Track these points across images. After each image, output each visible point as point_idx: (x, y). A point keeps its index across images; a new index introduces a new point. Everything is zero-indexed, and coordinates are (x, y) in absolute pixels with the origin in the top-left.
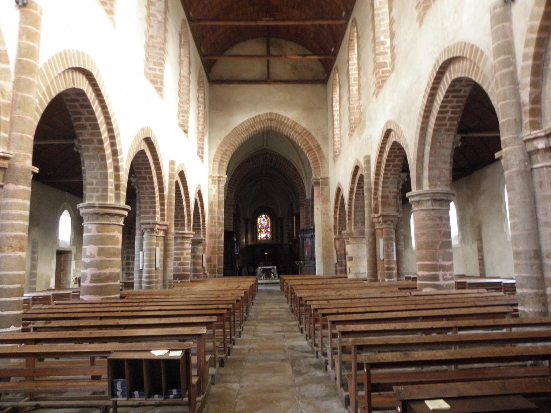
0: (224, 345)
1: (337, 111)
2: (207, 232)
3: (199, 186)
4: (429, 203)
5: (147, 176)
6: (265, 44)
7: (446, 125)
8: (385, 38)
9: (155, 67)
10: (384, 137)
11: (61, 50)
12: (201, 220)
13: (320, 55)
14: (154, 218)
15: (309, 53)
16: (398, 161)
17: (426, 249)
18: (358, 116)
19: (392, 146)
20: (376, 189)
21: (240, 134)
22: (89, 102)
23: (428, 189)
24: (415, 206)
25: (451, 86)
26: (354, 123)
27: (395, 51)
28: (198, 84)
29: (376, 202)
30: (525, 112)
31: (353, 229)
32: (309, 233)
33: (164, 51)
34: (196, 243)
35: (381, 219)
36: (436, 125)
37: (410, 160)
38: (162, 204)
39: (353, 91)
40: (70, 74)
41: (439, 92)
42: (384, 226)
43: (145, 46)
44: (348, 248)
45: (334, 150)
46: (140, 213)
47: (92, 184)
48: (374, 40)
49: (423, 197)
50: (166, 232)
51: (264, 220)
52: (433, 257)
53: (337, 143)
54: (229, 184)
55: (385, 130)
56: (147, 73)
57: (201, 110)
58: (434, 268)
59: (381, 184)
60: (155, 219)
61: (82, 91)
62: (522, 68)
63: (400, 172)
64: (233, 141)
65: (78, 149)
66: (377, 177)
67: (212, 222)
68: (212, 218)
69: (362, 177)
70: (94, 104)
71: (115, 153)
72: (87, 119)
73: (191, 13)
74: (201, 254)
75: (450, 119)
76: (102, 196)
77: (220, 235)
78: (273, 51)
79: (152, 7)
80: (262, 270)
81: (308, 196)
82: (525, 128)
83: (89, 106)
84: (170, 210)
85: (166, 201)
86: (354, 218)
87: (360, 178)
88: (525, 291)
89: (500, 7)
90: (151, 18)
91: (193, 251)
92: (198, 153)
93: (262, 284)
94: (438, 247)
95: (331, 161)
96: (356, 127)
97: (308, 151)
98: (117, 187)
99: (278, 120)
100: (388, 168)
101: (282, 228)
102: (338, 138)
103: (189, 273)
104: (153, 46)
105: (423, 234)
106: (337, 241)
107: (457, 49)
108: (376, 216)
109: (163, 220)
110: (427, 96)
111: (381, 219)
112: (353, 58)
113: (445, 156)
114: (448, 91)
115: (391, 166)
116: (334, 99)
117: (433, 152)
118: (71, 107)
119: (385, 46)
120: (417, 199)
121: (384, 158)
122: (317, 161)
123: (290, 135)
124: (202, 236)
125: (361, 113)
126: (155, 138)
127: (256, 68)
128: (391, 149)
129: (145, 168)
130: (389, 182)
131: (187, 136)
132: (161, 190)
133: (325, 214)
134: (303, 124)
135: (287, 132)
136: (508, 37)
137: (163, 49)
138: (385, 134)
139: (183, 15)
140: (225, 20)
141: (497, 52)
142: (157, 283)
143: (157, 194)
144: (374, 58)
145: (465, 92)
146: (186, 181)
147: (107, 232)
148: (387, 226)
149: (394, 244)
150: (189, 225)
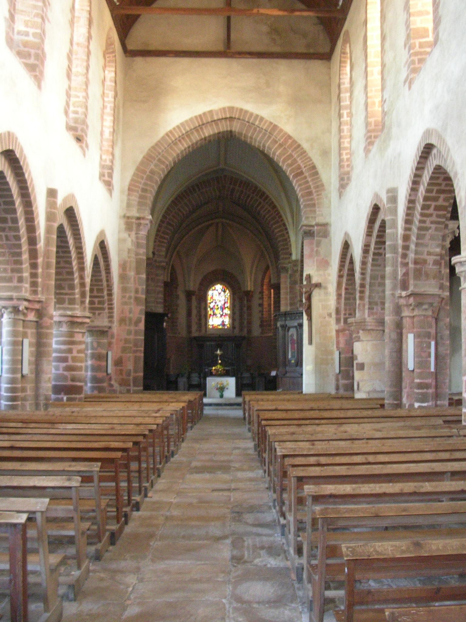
0: (118, 509)
5: (9, 216)
16: (444, 200)
20: (406, 248)
26: (374, 131)
29: (404, 270)
31: (366, 316)
35: (411, 300)
37: (460, 201)
38: (34, 266)
51: (220, 294)
55: (423, 145)
67: (124, 297)
68: (124, 290)
85: (40, 260)
86: (370, 297)
87: (380, 227)
92: (102, 175)
93: (210, 405)
96: (376, 137)
100: (426, 212)
101: (249, 308)
102: (346, 154)
108: (404, 294)
116: (342, 87)
121: (420, 194)
122: (310, 193)
123: (264, 146)
126: (22, 151)
128: (431, 178)
130: (428, 237)
135: (260, 142)
138: (422, 152)
142: (24, 399)
148: (421, 313)
149: (433, 343)
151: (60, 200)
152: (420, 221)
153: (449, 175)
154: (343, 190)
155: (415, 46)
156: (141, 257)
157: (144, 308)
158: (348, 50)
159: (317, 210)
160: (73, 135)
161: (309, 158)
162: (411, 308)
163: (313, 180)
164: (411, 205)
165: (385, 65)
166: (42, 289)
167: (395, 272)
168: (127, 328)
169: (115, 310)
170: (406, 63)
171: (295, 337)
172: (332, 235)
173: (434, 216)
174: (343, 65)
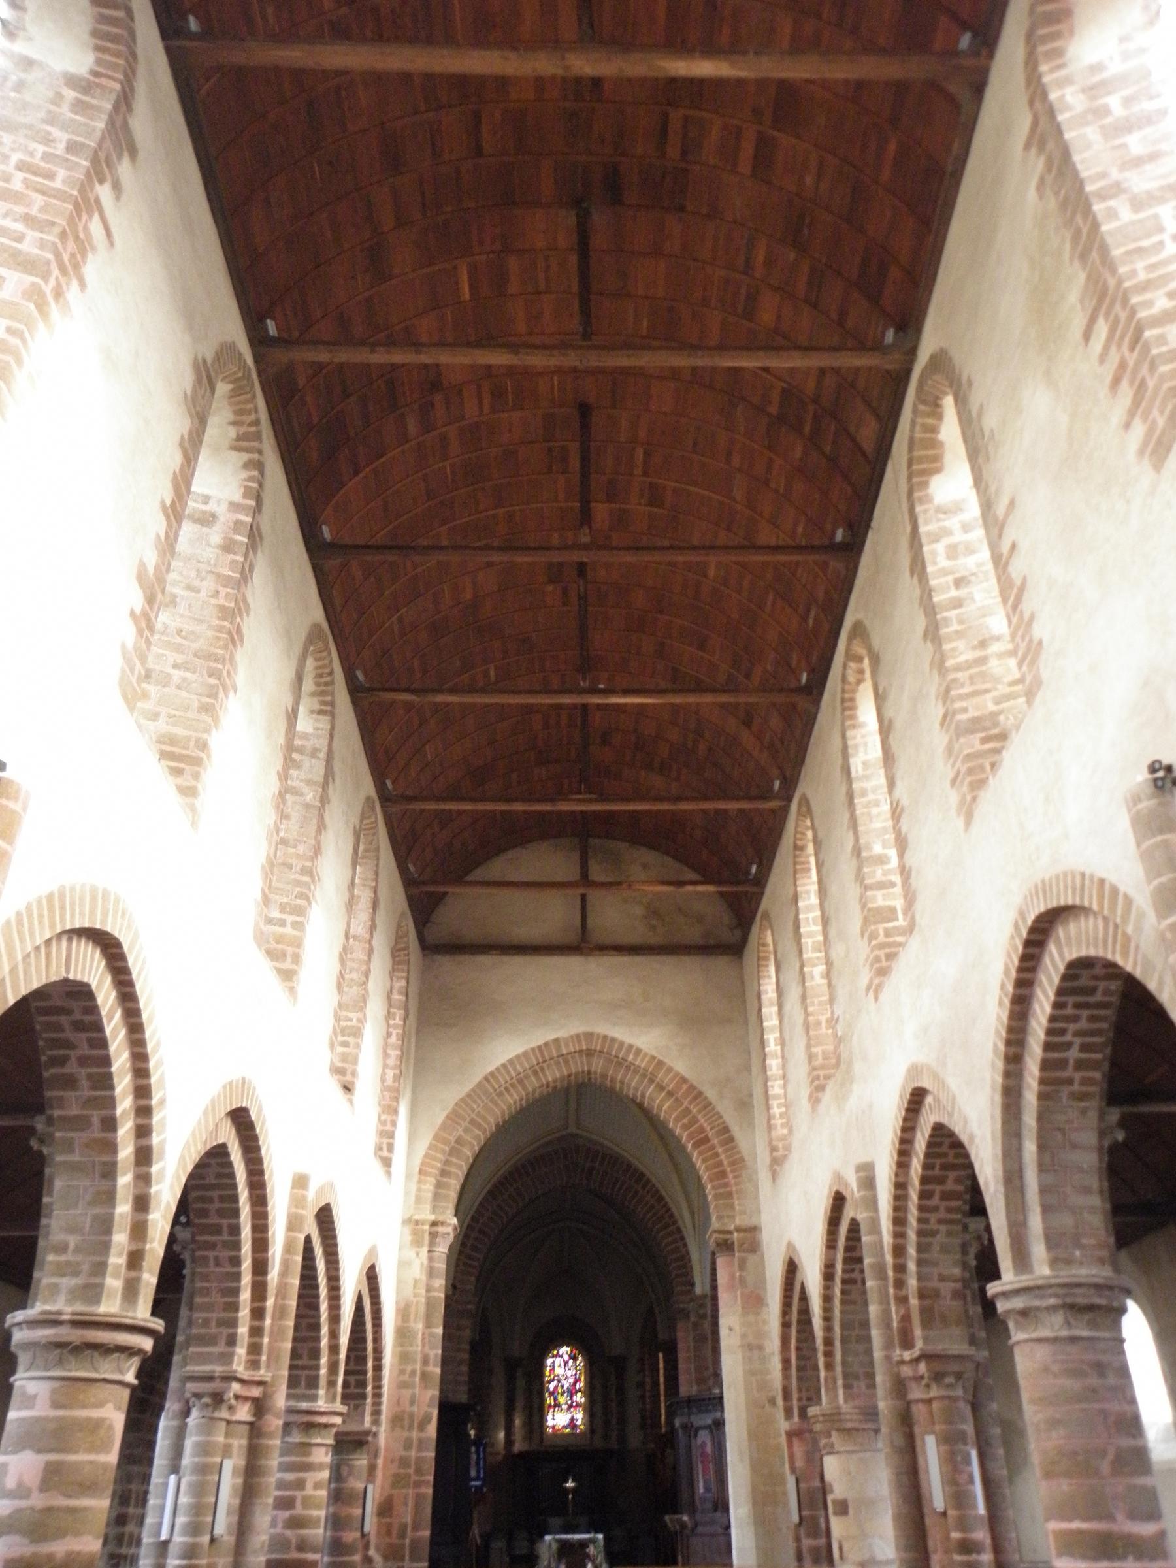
1: (772, 1029)
2: (384, 1408)
3: (373, 1251)
4: (1058, 1319)
5: (225, 1222)
6: (576, 857)
7: (1070, 1081)
8: (884, 847)
9: (283, 916)
10: (908, 1110)
11: (54, 887)
12: (370, 1364)
13: (719, 882)
14: (227, 1358)
15: (691, 875)
17: (1067, 1474)
18: (831, 1048)
19: (931, 1136)
20: (900, 1268)
21: (500, 1095)
22: (99, 1014)
23: (1046, 1271)
24: (1020, 1328)
25: (1065, 978)
26: (822, 1067)
27: (912, 881)
28: (393, 956)
29: (902, 1311)
32: (708, 1411)
33: (312, 876)
34: (350, 1443)
35: (922, 1367)
36: (1042, 1081)
37: (986, 1184)
38: (258, 1313)
39: (812, 978)
40: (64, 943)
41: (1039, 992)
42: (934, 1392)
43: (263, 867)
44: (832, 1466)
45: (770, 1141)
46: (188, 1343)
47: (62, 1249)
48: (857, 851)
49: (1036, 1297)
50: (260, 1407)
51: (566, 1363)
52: (1097, 1508)
53: (778, 1122)
54: (463, 1244)
55: (909, 1091)
56: (262, 933)
57: (396, 1026)
59: (912, 1251)
60: (230, 1363)
61: (87, 985)
63: (965, 1214)
64: (478, 1114)
65: (42, 1141)
66: (899, 1229)
68: (404, 1358)
69: (854, 1227)
70: (109, 1022)
71: (144, 1156)
72: (83, 1061)
73: (388, 783)
74: (360, 1486)
75: (1080, 1065)
76: (86, 1286)
77: (426, 1420)
78: (597, 873)
79: (293, 772)
80: (555, 1546)
81: (701, 1287)
83: (98, 1026)
84: (277, 1334)
85: (270, 1303)
86: (844, 1363)
90: (288, 796)
91: (338, 1474)
92: (379, 1148)
94: (1105, 1467)
95: (763, 1177)
96: (827, 1077)
97: (696, 1145)
98: (135, 1260)
99: (609, 1053)
101: (621, 1390)
102: (779, 1106)
103: (317, 1556)
104: (284, 864)
106: (796, 1442)
107: (1066, 887)
108: (907, 1355)
109: (254, 1364)
110: (1007, 1002)
111: (922, 1367)
112: (808, 892)
113: (1081, 1170)
114: (1060, 992)
115: (937, 1197)
116: (764, 997)
117: (1047, 1159)
118: (50, 1027)
119: (886, 867)
120: (1018, 1303)
122: (723, 1174)
123: (643, 1096)
124: (368, 1418)
125: (839, 1040)
126: (260, 1110)
127: (552, 915)
128: (930, 1145)
129: (222, 1199)
131: (351, 1101)
132: (260, 1267)
133: (753, 1347)
134: (681, 1066)
135: (636, 1089)
137: (309, 872)
139: (368, 787)
140: (473, 800)
143: (246, 1279)
144: (861, 898)
145: (1106, 992)
146: (335, 1237)
147: (84, 1407)
148: (943, 1392)
149: (974, 1454)
150: (332, 1384)
151: (311, 1194)
152: (920, 1220)
153: (957, 1137)
154: (778, 1168)
155: (878, 935)
156: (436, 1294)
157: (437, 1393)
158: (769, 940)
160: (339, 1081)
161: (718, 1113)
162: (924, 1383)
163: (726, 1151)
164: (899, 1192)
165: (832, 964)
166: (268, 1359)
167: (886, 1313)
168: (406, 1434)
169: (385, 1399)
170: (867, 960)
171: (709, 1449)
173: (942, 1209)
174: (763, 963)
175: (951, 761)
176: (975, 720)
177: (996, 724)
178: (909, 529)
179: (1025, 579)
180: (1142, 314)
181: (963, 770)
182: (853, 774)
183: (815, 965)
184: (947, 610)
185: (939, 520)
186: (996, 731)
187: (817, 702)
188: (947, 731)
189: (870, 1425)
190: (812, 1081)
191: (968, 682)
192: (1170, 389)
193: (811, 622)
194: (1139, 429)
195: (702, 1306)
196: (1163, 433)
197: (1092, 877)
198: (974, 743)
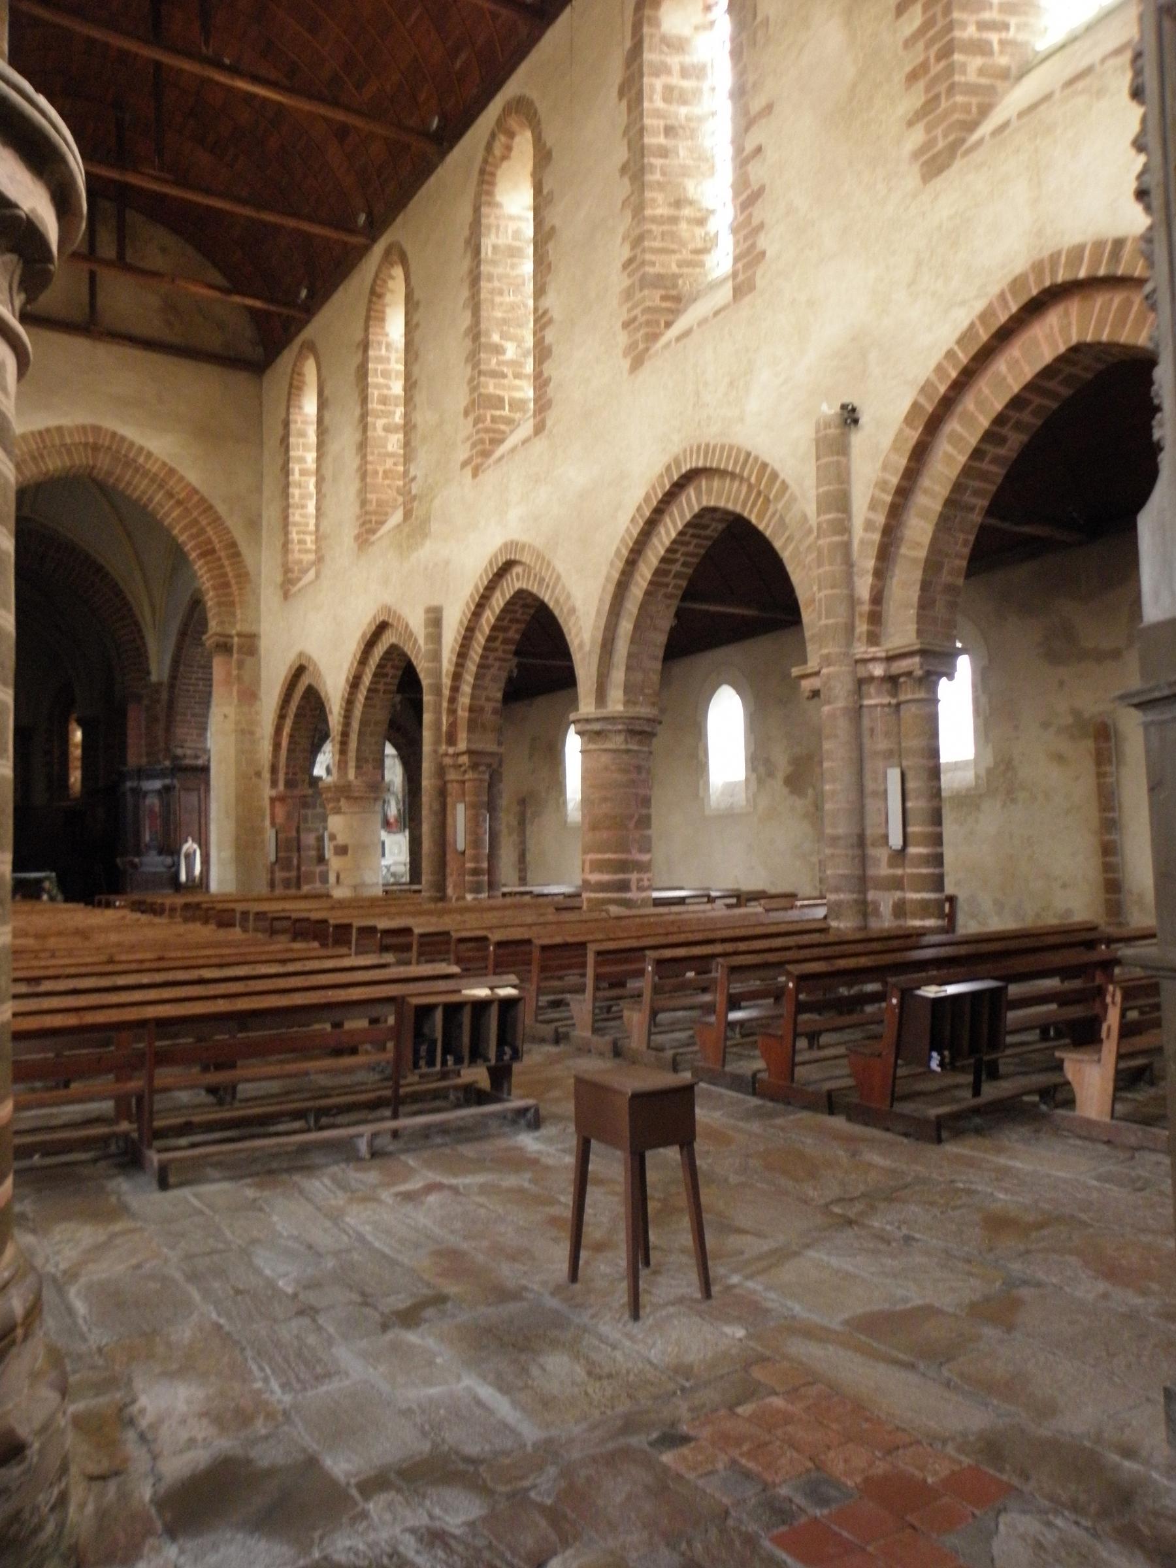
4: (620, 739)
17: (608, 828)
20: (455, 689)
23: (620, 708)
26: (375, 513)
29: (451, 719)
30: (861, 615)
37: (581, 645)
39: (375, 429)
58: (623, 866)
62: (862, 542)
75: (678, 575)
82: (859, 639)
86: (358, 750)
88: (842, 896)
89: (836, 427)
94: (631, 825)
99: (118, 451)
105: (605, 799)
106: (277, 804)
108: (451, 750)
111: (464, 759)
119: (501, 358)
122: (227, 585)
123: (150, 500)
130: (488, 678)
134: (193, 476)
135: (144, 493)
136: (842, 483)
141: (824, 503)
148: (476, 776)
159: (238, 612)
161: (226, 528)
170: (468, 438)
172: (263, 652)
175: (629, 305)
176: (660, 277)
177: (675, 286)
178: (628, 44)
179: (762, 189)
180: (957, 34)
181: (642, 319)
182: (483, 255)
183: (378, 417)
184: (655, 156)
185: (661, 52)
186: (673, 293)
187: (443, 154)
188: (629, 276)
189: (372, 795)
190: (364, 524)
191: (659, 237)
192: (958, 121)
193: (458, 65)
194: (917, 136)
195: (157, 692)
196: (939, 153)
197: (756, 459)
198: (653, 297)
